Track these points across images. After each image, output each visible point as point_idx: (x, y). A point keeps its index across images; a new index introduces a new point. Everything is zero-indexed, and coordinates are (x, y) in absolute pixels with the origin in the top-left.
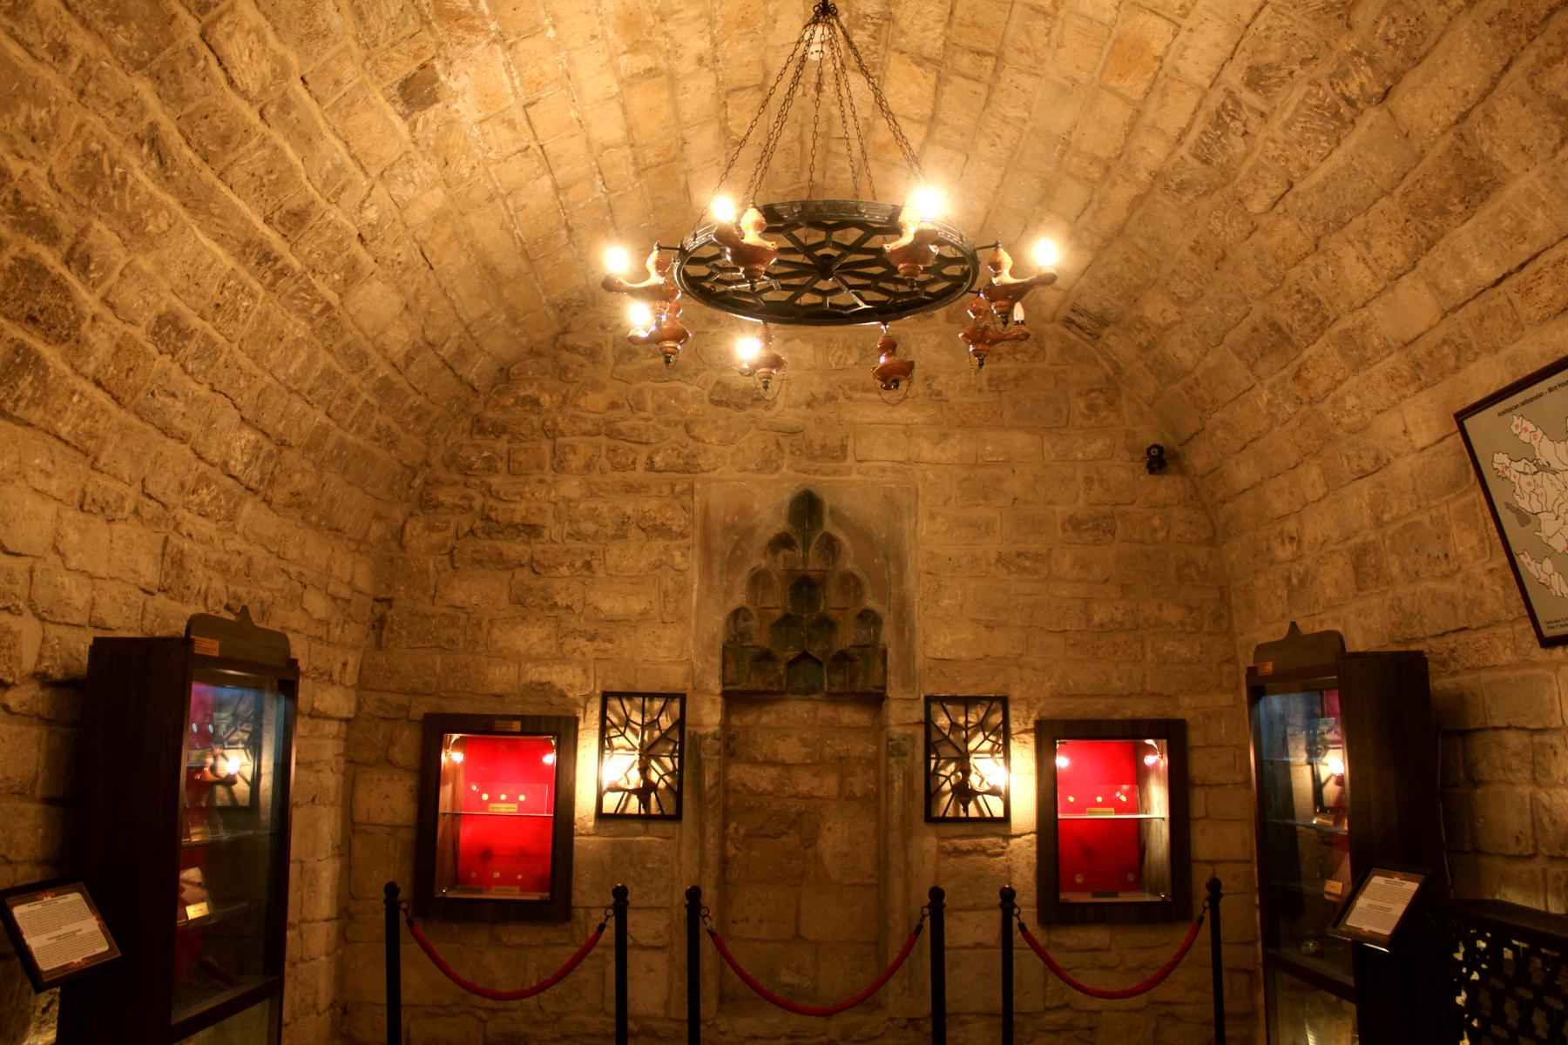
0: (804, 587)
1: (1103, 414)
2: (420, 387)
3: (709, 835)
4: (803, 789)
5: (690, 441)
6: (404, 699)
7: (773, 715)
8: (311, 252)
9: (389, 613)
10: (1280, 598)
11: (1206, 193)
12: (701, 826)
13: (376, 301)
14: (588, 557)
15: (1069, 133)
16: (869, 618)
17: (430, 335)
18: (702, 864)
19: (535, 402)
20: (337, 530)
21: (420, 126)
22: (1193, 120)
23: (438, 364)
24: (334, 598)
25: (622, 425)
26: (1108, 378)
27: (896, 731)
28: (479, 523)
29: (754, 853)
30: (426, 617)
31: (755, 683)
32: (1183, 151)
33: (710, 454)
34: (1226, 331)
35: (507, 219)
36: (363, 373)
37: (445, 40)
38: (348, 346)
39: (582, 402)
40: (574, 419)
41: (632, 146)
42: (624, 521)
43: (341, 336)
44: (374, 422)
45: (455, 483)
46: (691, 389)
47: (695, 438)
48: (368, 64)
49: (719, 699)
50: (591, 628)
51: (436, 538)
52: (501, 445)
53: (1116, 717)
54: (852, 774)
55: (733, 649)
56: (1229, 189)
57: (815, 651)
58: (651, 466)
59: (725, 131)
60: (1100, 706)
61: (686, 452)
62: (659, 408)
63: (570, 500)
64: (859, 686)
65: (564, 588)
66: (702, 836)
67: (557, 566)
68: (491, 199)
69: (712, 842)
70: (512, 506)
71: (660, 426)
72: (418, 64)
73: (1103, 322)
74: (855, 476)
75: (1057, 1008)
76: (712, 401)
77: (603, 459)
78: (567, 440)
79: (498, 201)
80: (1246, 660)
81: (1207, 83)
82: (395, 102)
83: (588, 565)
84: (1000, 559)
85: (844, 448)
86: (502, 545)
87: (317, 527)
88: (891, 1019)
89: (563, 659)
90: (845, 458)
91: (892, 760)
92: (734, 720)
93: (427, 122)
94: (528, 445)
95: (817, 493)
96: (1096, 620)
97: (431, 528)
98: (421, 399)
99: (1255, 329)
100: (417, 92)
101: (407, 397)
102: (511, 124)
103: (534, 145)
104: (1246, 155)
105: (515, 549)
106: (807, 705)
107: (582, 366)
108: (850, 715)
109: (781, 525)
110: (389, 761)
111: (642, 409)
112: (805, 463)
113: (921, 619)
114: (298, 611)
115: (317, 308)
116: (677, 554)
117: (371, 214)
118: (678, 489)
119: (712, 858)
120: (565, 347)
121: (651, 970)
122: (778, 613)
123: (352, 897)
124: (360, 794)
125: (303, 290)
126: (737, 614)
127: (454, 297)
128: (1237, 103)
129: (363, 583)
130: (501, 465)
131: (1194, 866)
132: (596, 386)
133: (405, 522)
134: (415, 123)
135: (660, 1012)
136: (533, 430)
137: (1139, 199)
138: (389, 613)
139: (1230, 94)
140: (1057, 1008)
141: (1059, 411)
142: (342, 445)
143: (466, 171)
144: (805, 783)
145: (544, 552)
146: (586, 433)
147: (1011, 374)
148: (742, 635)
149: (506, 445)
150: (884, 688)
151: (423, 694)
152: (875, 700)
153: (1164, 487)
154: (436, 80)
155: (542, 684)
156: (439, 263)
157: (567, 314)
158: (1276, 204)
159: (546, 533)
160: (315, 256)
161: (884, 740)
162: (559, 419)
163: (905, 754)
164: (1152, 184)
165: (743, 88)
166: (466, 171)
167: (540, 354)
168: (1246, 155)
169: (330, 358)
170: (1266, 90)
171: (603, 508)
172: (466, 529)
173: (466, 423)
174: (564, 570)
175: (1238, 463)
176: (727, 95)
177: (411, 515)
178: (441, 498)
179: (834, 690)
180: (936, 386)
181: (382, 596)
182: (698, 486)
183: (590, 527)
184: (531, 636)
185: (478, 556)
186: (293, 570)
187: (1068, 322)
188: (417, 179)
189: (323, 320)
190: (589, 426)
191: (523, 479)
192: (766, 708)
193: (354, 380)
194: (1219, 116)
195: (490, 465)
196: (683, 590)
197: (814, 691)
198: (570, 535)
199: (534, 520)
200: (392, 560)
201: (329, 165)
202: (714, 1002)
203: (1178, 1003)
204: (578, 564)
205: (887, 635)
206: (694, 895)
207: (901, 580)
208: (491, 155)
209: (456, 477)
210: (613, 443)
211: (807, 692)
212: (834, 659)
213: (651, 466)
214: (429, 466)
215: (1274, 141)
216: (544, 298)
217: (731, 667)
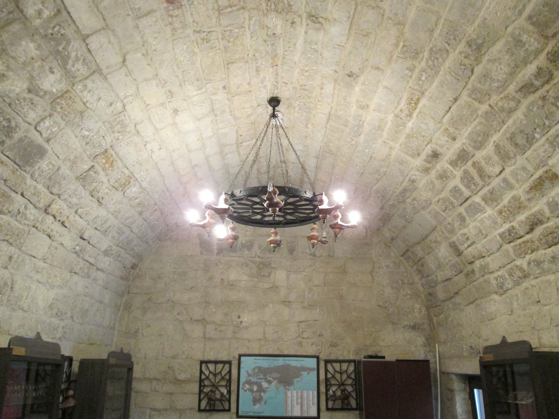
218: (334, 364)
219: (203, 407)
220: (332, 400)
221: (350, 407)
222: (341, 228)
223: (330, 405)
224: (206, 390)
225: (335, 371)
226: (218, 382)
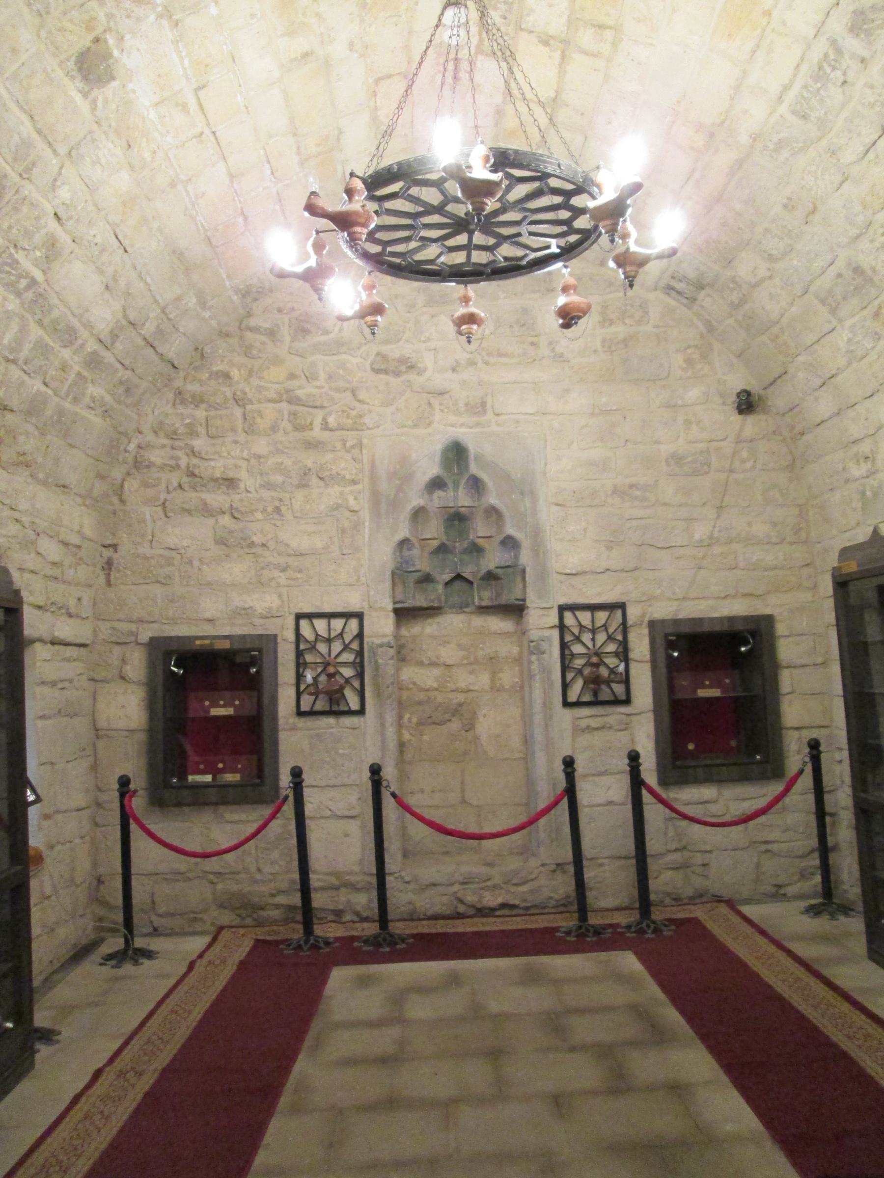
0: (457, 519)
1: (699, 366)
2: (127, 362)
3: (388, 725)
4: (462, 684)
5: (357, 404)
6: (133, 627)
7: (435, 627)
8: (10, 227)
9: (115, 556)
10: (855, 509)
11: (801, 150)
12: (381, 717)
13: (79, 284)
14: (277, 504)
15: (678, 102)
16: (510, 543)
17: (132, 316)
18: (384, 748)
19: (227, 376)
20: (64, 486)
21: (100, 104)
22: (795, 75)
23: (141, 342)
24: (66, 544)
25: (300, 393)
26: (702, 336)
27: (534, 634)
28: (185, 479)
29: (425, 738)
30: (146, 558)
31: (420, 601)
32: (783, 109)
34: (812, 281)
35: (190, 206)
36: (74, 347)
37: (115, 12)
38: (56, 322)
39: (265, 374)
40: (260, 389)
41: (295, 135)
42: (306, 472)
43: (49, 312)
44: (89, 392)
45: (163, 446)
46: (355, 361)
47: (359, 401)
48: (43, 34)
49: (392, 615)
50: (282, 560)
51: (150, 492)
52: (201, 413)
53: (716, 615)
54: (501, 671)
55: (399, 574)
56: (824, 142)
57: (467, 572)
58: (325, 427)
59: (375, 119)
60: (702, 607)
61: (354, 413)
62: (330, 377)
63: (260, 457)
64: (504, 600)
65: (259, 529)
66: (383, 725)
67: (252, 512)
68: (173, 185)
69: (391, 731)
70: (213, 464)
71: (332, 393)
72: (90, 37)
73: (700, 286)
74: (494, 428)
75: (676, 850)
76: (373, 370)
77: (285, 422)
78: (256, 407)
79: (180, 187)
80: (833, 561)
81: (812, 32)
82: (73, 78)
83: (277, 510)
84: (615, 491)
85: (483, 404)
86: (208, 497)
87: (44, 483)
88: (543, 865)
89: (261, 584)
90: (484, 412)
91: (533, 658)
92: (404, 632)
93: (106, 101)
94: (224, 412)
96: (697, 537)
97: (145, 485)
98: (129, 373)
99: (839, 275)
100: (93, 66)
101: (116, 371)
102: (184, 107)
103: (207, 132)
104: (844, 105)
105: (216, 499)
106: (462, 617)
107: (263, 343)
108: (497, 624)
109: (433, 469)
110: (122, 678)
111: (317, 379)
112: (452, 418)
113: (553, 545)
114: (33, 555)
115: (23, 283)
117: (64, 193)
118: (348, 444)
119: (392, 744)
120: (250, 329)
121: (347, 835)
122: (435, 543)
123: (100, 790)
124: (101, 706)
125: (6, 264)
126: (404, 543)
127: (149, 280)
128: (839, 51)
129: (88, 532)
130: (202, 430)
131: (784, 731)
132: (277, 361)
133: (124, 480)
134: (95, 101)
135: (356, 869)
136: (226, 400)
137: (740, 163)
138: (115, 556)
139: (833, 42)
140: (676, 850)
141: (661, 365)
142: (61, 412)
143: (147, 155)
144: (463, 679)
145: (241, 500)
146: (270, 401)
147: (621, 337)
148: (407, 562)
149: (204, 413)
150: (524, 600)
151: (148, 622)
152: (516, 610)
153: (751, 424)
154: (110, 55)
155: (245, 609)
156: (132, 246)
157: (249, 300)
158: (868, 151)
159: (242, 485)
160: (14, 231)
161: (525, 643)
162: (247, 390)
163: (543, 653)
164: (752, 147)
165: (389, 76)
166: (147, 155)
167: (227, 335)
168: (844, 105)
169: (41, 332)
170: (869, 33)
171: (288, 462)
172: (175, 484)
173: (170, 396)
174: (259, 515)
175: (817, 399)
176: (377, 81)
177: (128, 474)
178: (153, 459)
179: (484, 604)
180: (559, 349)
181: (109, 542)
182: (365, 441)
183: (279, 479)
184: (236, 570)
185: (186, 506)
186: (26, 520)
187: (669, 289)
188: (103, 161)
189: (29, 295)
190: (272, 395)
191: (219, 441)
192: (430, 620)
193: (66, 353)
194: (820, 68)
195: (192, 432)
196: (357, 527)
197: (467, 606)
198: (262, 486)
199: (231, 475)
200: (115, 513)
201: (16, 138)
202: (399, 856)
203: (774, 842)
204: (270, 509)
205: (525, 558)
206: (375, 770)
207: (535, 512)
208: (169, 139)
209: (165, 441)
210: (294, 408)
211: (461, 608)
213: (325, 427)
214: (140, 432)
215: (871, 87)
216: (228, 283)
217: (399, 589)
218: (578, 613)
219: (572, 697)
220: (311, 694)
221: (343, 708)
222: (642, 262)
223: (307, 702)
224: (579, 662)
225: (581, 626)
226: (594, 646)
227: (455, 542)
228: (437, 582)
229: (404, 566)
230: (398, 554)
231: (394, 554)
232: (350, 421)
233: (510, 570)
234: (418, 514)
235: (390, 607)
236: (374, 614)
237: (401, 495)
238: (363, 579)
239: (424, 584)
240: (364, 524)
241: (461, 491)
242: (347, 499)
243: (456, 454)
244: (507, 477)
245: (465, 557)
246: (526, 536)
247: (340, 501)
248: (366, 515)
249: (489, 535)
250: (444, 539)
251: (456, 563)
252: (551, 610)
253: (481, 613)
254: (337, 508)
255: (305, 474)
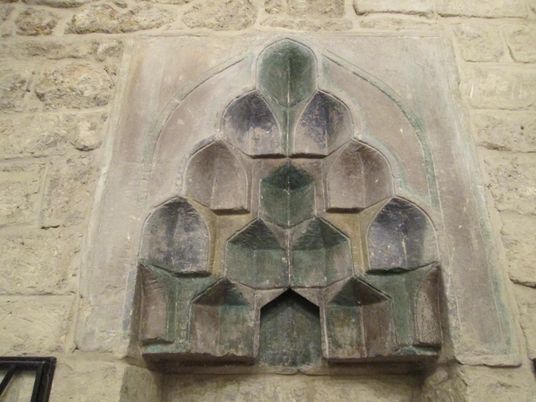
0: (288, 180)
16: (401, 217)
31: (206, 341)
33: (154, 10)
57: (307, 286)
64: (387, 347)
95: (304, 50)
106: (297, 383)
109: (245, 81)
116: (84, 126)
118: (101, 49)
122: (242, 222)
126: (174, 211)
148: (181, 254)
179: (342, 354)
196: (84, 176)
197: (306, 359)
205: (438, 245)
207: (448, 157)
212: (339, 300)
227: (284, 227)
228: (244, 303)
229: (174, 261)
230: (162, 233)
231: (153, 229)
232: (116, 22)
233: (401, 279)
234: (211, 157)
235: (122, 348)
236: (81, 365)
237: (180, 122)
238: (73, 282)
239: (220, 309)
240: (98, 170)
241: (298, 131)
242: (76, 128)
243: (291, 65)
244: (387, 96)
245: (304, 256)
246: (435, 201)
247: (63, 132)
248: (105, 155)
249: (350, 205)
250: (262, 214)
251: (285, 267)
252: (514, 372)
253: (335, 376)
254: (55, 143)
255: (13, 89)
